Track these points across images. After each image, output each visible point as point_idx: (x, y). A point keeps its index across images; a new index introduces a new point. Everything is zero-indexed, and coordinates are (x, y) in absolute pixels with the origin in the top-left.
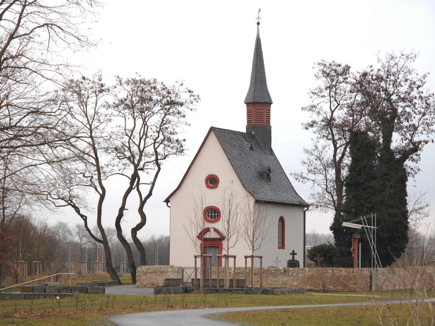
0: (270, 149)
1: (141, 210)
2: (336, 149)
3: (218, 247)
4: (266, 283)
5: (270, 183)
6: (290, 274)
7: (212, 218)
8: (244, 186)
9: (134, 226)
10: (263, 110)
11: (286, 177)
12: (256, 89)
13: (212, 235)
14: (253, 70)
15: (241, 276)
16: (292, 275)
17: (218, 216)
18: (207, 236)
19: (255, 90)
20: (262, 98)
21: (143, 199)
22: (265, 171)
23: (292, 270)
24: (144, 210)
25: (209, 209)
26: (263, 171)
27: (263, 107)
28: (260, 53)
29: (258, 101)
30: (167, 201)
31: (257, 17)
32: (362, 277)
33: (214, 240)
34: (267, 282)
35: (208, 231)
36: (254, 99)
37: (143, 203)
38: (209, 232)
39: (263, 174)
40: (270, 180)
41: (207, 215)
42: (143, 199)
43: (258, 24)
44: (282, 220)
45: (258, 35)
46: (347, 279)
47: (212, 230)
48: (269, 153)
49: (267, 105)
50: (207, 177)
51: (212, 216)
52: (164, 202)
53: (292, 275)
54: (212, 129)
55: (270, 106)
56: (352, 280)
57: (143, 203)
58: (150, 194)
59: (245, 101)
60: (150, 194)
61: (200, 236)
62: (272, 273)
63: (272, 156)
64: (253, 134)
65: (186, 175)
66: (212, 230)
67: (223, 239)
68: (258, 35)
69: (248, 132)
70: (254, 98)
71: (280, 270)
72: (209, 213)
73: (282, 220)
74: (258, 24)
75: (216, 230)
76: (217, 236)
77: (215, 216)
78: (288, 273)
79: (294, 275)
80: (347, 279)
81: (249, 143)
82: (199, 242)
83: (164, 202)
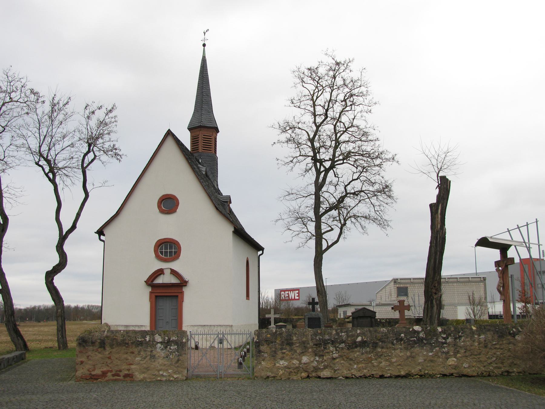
1: (60, 248)
3: (177, 296)
4: (388, 363)
7: (166, 255)
9: (50, 268)
10: (211, 136)
13: (167, 279)
14: (99, 231)
15: (331, 348)
17: (175, 252)
18: (160, 280)
20: (210, 122)
21: (64, 233)
22: (226, 200)
23: (442, 331)
24: (84, 196)
25: (163, 243)
26: (224, 200)
27: (211, 133)
28: (207, 75)
29: (206, 125)
30: (100, 232)
34: (391, 362)
35: (160, 274)
37: (63, 238)
38: (162, 275)
39: (224, 203)
41: (159, 251)
42: (64, 233)
43: (204, 45)
47: (167, 272)
50: (160, 199)
51: (166, 252)
52: (95, 233)
57: (63, 238)
58: (74, 227)
60: (74, 227)
61: (150, 282)
62: (401, 339)
65: (113, 220)
67: (185, 284)
72: (162, 249)
74: (204, 45)
75: (174, 272)
76: (174, 280)
77: (171, 252)
78: (437, 339)
83: (95, 233)
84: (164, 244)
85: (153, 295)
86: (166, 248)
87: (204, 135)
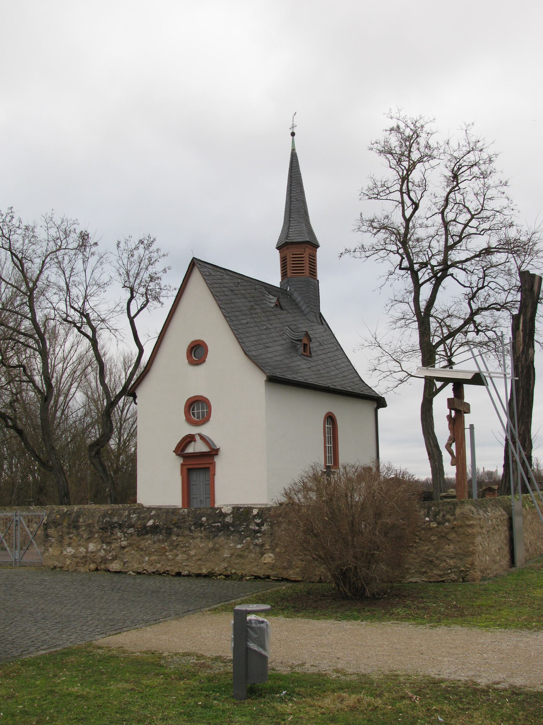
0: (318, 315)
2: (417, 286)
5: (310, 359)
6: (253, 527)
8: (246, 354)
10: (303, 254)
11: (345, 357)
12: (291, 225)
13: (198, 447)
15: (119, 534)
16: (259, 531)
18: (190, 449)
19: (289, 226)
20: (300, 236)
31: (290, 126)
32: (484, 531)
33: (202, 455)
34: (188, 555)
36: (289, 238)
38: (193, 443)
40: (310, 353)
41: (191, 412)
43: (293, 134)
44: (330, 419)
45: (293, 150)
46: (433, 538)
48: (316, 321)
49: (309, 246)
53: (259, 531)
54: (194, 263)
55: (316, 251)
56: (450, 541)
59: (451, 463)
62: (201, 525)
63: (322, 326)
64: (288, 290)
66: (197, 438)
67: (214, 453)
68: (293, 150)
69: (282, 287)
70: (288, 236)
71: (225, 515)
73: (330, 419)
74: (293, 134)
75: (202, 437)
78: (248, 526)
79: (264, 528)
80: (433, 538)
81: (274, 297)
82: (178, 462)
84: (195, 404)
85: (185, 468)
86: (198, 409)
87: (293, 254)
